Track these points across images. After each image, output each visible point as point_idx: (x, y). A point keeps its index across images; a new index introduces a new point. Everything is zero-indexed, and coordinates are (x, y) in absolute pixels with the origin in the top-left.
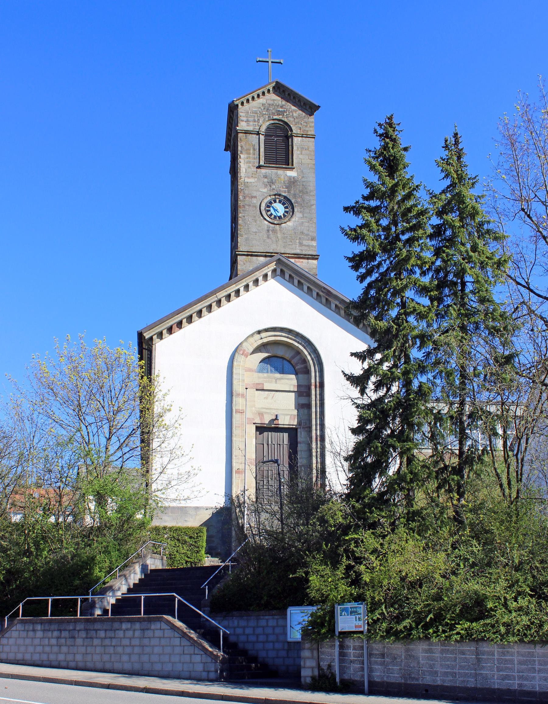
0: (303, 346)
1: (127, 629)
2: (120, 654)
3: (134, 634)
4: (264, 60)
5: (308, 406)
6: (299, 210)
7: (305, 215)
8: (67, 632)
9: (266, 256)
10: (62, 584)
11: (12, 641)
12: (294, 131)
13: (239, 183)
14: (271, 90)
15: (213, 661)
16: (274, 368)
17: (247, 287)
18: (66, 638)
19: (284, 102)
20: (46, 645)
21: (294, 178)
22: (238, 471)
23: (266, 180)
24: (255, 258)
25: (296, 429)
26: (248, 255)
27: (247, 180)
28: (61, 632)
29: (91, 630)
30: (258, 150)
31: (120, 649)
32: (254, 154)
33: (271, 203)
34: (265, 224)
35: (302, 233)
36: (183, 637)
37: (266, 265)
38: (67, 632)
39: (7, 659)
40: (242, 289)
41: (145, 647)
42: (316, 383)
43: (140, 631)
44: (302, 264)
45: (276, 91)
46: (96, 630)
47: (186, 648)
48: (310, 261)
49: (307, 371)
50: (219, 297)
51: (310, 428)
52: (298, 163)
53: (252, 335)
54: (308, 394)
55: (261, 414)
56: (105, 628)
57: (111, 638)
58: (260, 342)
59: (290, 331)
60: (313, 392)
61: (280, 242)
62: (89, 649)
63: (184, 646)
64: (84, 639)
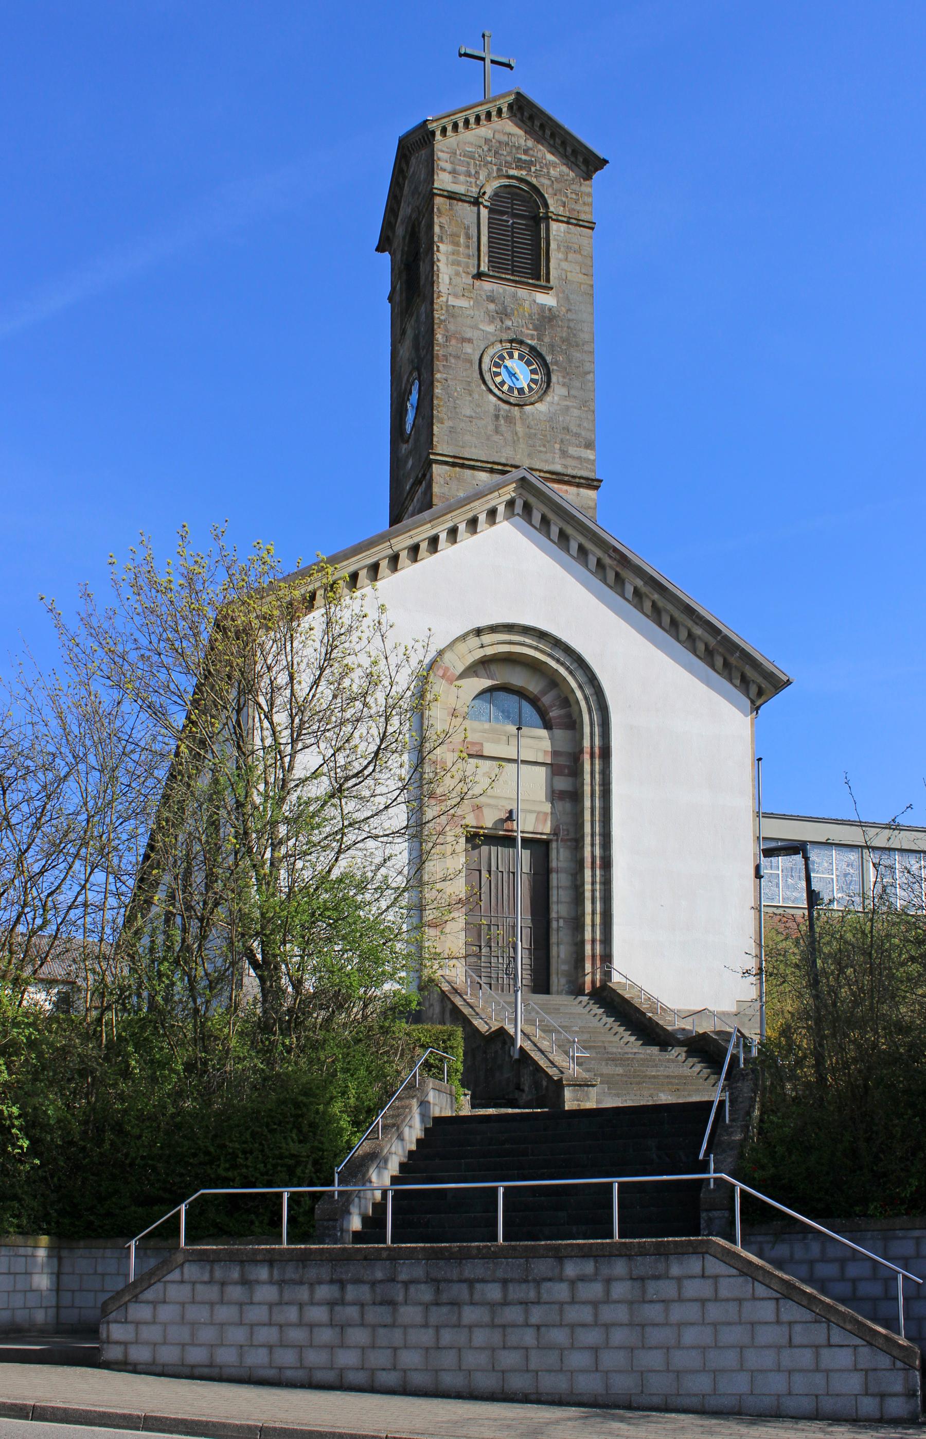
0: (567, 669)
1: (582, 1279)
2: (562, 1350)
3: (607, 1292)
4: (476, 53)
5: (575, 796)
6: (561, 379)
7: (573, 392)
8: (366, 1288)
9: (492, 471)
10: (251, 1152)
11: (166, 1313)
12: (552, 209)
13: (435, 307)
14: (505, 110)
15: (899, 1364)
16: (503, 712)
17: (453, 533)
18: (362, 1305)
19: (530, 143)
20: (291, 1325)
21: (550, 310)
23: (492, 307)
24: (468, 472)
25: (546, 844)
26: (454, 465)
27: (452, 301)
28: (343, 1288)
29: (451, 1281)
30: (475, 239)
31: (559, 1336)
32: (468, 247)
33: (502, 358)
34: (489, 402)
35: (567, 429)
36: (786, 1297)
37: (498, 487)
38: (366, 1288)
39: (154, 1363)
40: (443, 536)
41: (648, 1329)
42: (592, 748)
43: (629, 1283)
44: (568, 495)
45: (515, 116)
46: (471, 1283)
47: (798, 1328)
48: (582, 490)
49: (573, 724)
50: (396, 549)
52: (559, 278)
53: (464, 637)
54: (576, 771)
56: (500, 1274)
57: (525, 1303)
59: (542, 635)
60: (587, 767)
61: (522, 445)
62: (447, 1337)
63: (790, 1324)
64: (427, 1306)
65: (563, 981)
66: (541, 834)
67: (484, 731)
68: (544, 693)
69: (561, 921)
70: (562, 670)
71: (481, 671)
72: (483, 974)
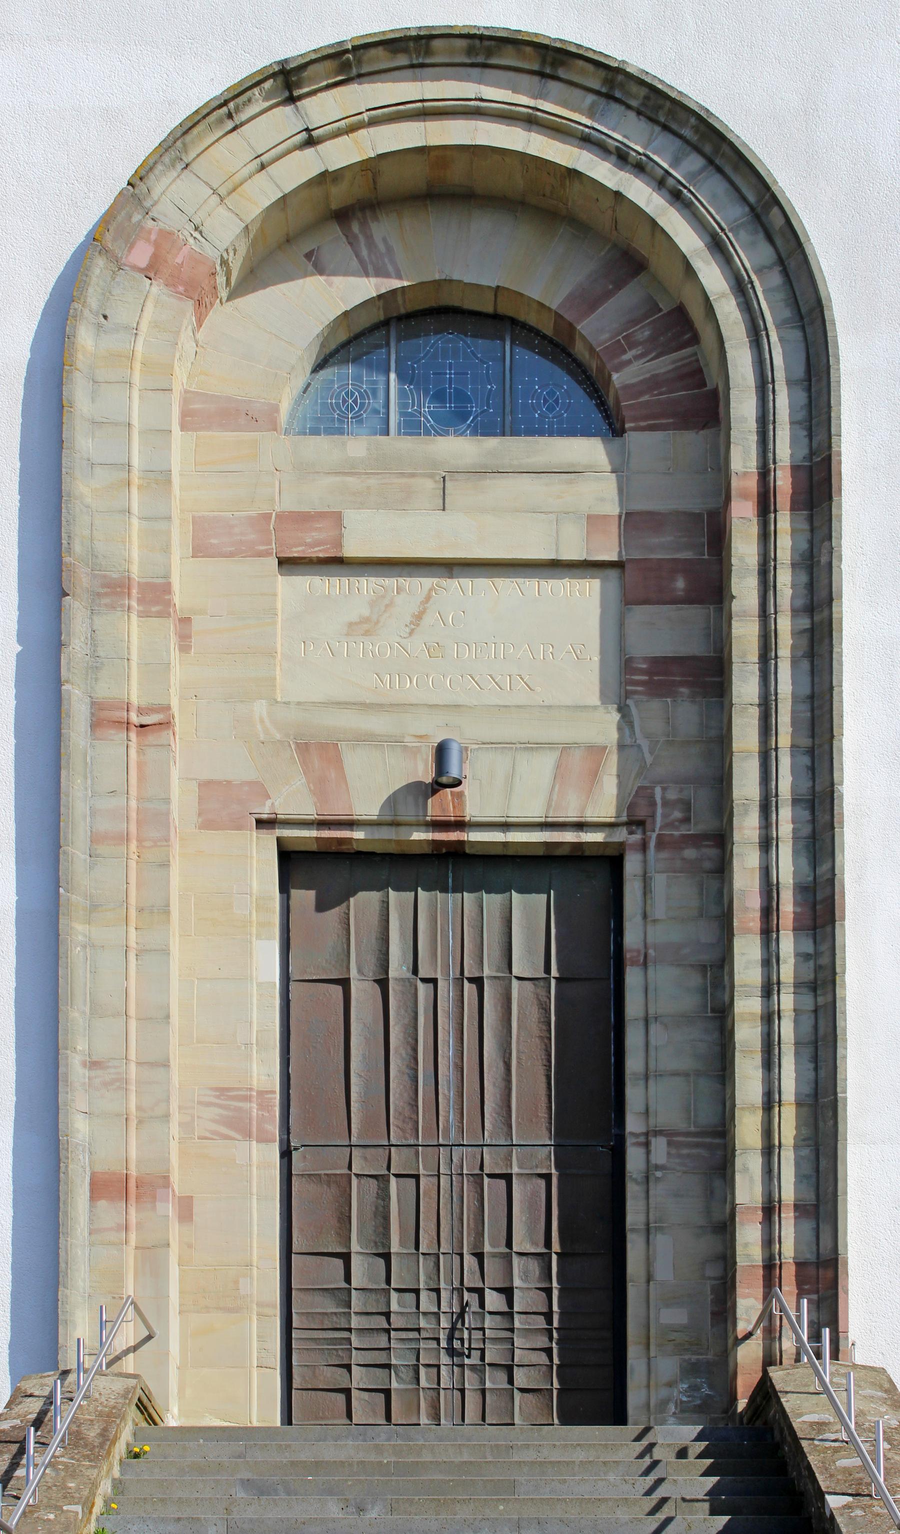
0: (661, 182)
16: (439, 397)
22: (109, 1187)
25: (611, 862)
42: (765, 473)
49: (703, 408)
51: (721, 840)
53: (227, 109)
55: (319, 752)
58: (303, 167)
65: (668, 1366)
66: (580, 826)
67: (349, 469)
68: (589, 301)
69: (659, 1145)
70: (640, 193)
71: (331, 241)
72: (356, 1357)
